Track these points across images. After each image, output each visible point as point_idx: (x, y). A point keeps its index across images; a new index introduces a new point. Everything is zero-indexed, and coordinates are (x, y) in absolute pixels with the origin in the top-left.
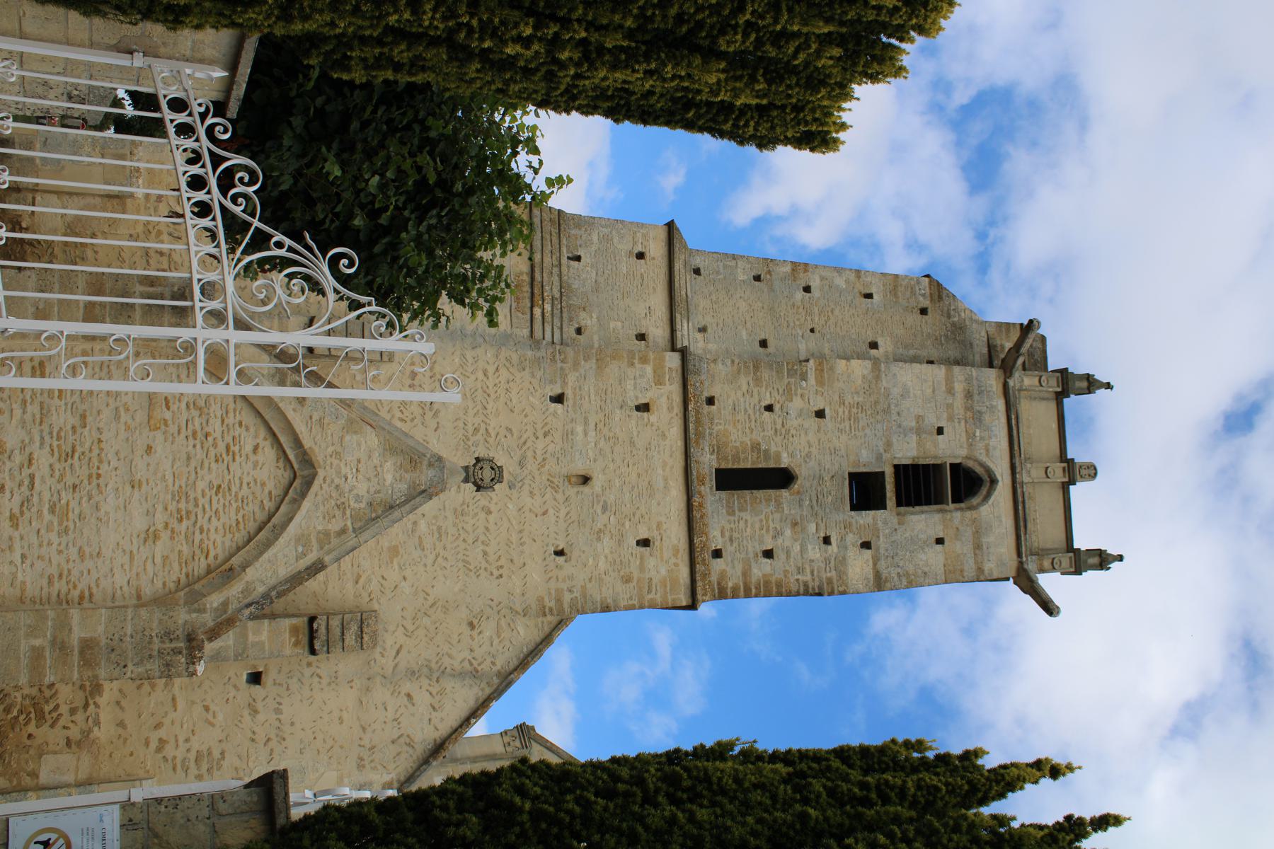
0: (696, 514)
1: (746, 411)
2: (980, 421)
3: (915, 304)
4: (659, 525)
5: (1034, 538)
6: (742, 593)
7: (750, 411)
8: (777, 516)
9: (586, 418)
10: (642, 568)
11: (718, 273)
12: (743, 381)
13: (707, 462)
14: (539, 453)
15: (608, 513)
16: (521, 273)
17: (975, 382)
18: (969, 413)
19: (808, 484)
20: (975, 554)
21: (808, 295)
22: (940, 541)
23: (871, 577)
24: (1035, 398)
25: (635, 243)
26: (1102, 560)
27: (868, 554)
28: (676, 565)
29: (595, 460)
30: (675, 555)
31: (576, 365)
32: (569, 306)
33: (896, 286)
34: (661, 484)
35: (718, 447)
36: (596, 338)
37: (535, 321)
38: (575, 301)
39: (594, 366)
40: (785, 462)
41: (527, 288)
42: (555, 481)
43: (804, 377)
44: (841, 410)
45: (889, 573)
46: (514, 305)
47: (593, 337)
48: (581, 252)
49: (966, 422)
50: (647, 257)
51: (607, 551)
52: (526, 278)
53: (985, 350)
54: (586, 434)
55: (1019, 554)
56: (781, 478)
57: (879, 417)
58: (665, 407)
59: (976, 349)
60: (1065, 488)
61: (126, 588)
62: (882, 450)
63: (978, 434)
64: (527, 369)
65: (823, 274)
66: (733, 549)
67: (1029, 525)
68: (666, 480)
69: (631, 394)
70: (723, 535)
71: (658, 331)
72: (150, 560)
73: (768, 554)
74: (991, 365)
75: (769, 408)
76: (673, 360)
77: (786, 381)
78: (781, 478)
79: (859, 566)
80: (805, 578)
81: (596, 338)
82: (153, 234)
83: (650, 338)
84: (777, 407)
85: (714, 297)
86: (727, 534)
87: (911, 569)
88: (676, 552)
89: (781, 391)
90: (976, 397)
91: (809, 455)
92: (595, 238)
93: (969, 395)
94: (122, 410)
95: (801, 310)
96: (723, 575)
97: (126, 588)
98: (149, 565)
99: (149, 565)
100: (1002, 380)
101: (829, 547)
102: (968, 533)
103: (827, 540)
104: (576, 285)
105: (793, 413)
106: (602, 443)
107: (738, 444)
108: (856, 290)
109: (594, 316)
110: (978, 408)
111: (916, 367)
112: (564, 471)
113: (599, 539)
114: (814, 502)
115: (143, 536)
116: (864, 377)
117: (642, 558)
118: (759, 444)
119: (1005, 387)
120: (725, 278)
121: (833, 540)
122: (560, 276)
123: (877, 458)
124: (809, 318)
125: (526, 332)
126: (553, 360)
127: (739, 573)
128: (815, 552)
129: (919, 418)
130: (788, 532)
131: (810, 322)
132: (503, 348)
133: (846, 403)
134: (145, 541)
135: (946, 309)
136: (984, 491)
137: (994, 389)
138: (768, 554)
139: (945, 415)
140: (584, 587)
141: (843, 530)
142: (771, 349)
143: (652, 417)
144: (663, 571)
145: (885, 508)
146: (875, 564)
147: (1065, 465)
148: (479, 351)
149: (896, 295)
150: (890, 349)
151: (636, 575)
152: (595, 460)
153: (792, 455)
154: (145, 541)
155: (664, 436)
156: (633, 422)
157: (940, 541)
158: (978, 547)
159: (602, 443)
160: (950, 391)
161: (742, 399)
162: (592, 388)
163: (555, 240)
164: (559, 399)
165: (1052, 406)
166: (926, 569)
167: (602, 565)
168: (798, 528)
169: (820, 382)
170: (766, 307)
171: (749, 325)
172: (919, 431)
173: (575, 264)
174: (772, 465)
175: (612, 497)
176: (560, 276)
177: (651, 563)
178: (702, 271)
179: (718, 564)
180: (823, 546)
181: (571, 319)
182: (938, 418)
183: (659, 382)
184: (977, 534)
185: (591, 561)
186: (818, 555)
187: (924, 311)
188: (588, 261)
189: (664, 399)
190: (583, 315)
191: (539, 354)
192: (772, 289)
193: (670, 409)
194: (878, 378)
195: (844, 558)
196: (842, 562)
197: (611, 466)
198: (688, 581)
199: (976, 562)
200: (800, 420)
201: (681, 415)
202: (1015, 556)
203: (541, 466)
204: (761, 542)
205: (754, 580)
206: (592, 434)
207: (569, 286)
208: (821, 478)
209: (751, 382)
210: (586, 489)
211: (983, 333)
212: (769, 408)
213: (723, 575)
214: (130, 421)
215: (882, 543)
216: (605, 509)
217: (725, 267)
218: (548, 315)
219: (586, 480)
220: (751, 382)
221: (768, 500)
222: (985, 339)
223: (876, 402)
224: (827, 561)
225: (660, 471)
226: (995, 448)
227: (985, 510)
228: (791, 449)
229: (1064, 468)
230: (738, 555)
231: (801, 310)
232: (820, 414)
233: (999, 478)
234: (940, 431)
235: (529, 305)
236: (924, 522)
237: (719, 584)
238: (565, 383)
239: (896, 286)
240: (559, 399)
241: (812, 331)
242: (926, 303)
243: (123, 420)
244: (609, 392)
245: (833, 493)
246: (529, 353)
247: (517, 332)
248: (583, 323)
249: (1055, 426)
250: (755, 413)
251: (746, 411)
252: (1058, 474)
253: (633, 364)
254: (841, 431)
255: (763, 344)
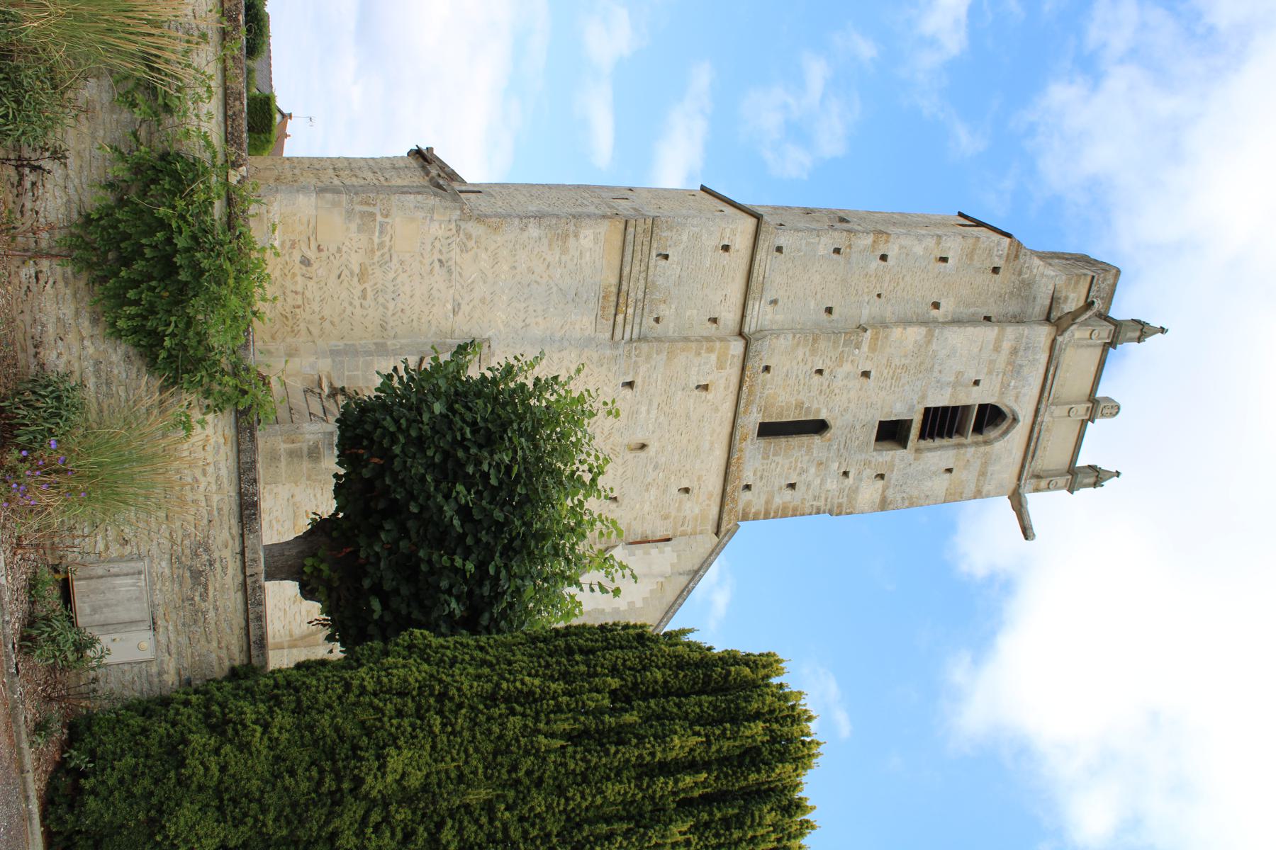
0: (733, 468)
1: (797, 376)
2: (1018, 373)
3: (989, 265)
4: (699, 478)
5: (1040, 461)
6: (762, 516)
7: (801, 377)
8: (806, 458)
9: (651, 400)
10: (679, 509)
11: (799, 250)
12: (800, 353)
13: (752, 419)
14: (606, 429)
15: (658, 471)
16: (610, 286)
17: (1024, 340)
18: (1009, 367)
19: (840, 432)
20: (978, 480)
21: (883, 263)
22: (949, 470)
23: (878, 501)
24: (1082, 346)
25: (722, 238)
26: (1097, 476)
27: (880, 483)
28: (709, 505)
29: (653, 432)
30: (709, 499)
31: (648, 358)
32: (651, 301)
33: (974, 249)
34: (707, 445)
35: (765, 407)
36: (672, 325)
37: (627, 244)
38: (657, 296)
39: (665, 358)
40: (823, 415)
41: (613, 298)
42: (617, 449)
43: (858, 346)
44: (886, 371)
45: (895, 498)
46: (600, 313)
47: (670, 326)
48: (669, 252)
49: (1004, 374)
50: (732, 250)
51: (652, 498)
52: (614, 289)
53: (1047, 302)
54: (648, 412)
55: (1019, 479)
56: (819, 427)
57: (921, 376)
58: (722, 386)
59: (1039, 301)
60: (1083, 424)
61: (282, 631)
62: (915, 402)
63: (1012, 384)
64: (605, 366)
65: (903, 243)
66: (761, 484)
67: (1038, 453)
68: (712, 443)
69: (695, 378)
70: (755, 474)
71: (729, 317)
72: (298, 614)
73: (792, 486)
74: (1048, 319)
75: (820, 372)
76: (737, 347)
77: (840, 350)
78: (819, 427)
79: (870, 492)
80: (819, 504)
81: (672, 325)
82: (289, 277)
83: (721, 322)
84: (826, 373)
85: (790, 273)
86: (759, 474)
87: (915, 493)
88: (710, 496)
89: (834, 358)
90: (1021, 353)
91: (846, 410)
92: (685, 238)
93: (1014, 351)
94: (274, 522)
95: (873, 278)
96: (749, 504)
97: (282, 631)
98: (298, 616)
99: (298, 616)
100: (1052, 336)
101: (847, 480)
102: (976, 465)
103: (846, 474)
104: (660, 281)
105: (840, 376)
106: (662, 418)
107: (784, 404)
108: (932, 256)
109: (673, 307)
110: (1020, 362)
111: (970, 330)
112: (626, 442)
113: (647, 490)
114: (842, 446)
115: (292, 599)
116: (916, 342)
117: (680, 502)
118: (803, 403)
119: (1054, 341)
120: (805, 255)
121: (851, 475)
122: (646, 279)
123: (909, 410)
124: (878, 285)
125: (608, 335)
126: (629, 356)
127: (763, 502)
128: (832, 484)
129: (959, 374)
130: (813, 470)
131: (878, 288)
132: (586, 350)
133: (893, 366)
134: (294, 602)
135: (1019, 267)
136: (1004, 426)
137: (1042, 345)
138: (792, 486)
139: (985, 370)
140: (629, 524)
141: (862, 468)
142: (835, 315)
143: (710, 396)
144: (697, 511)
145: (905, 447)
146: (884, 491)
147: (1090, 405)
148: (564, 353)
149: (971, 259)
150: (951, 309)
151: (673, 514)
152: (653, 432)
153: (831, 410)
154: (294, 602)
155: (717, 410)
156: (692, 401)
157: (949, 470)
158: (983, 474)
159: (662, 418)
160: (997, 349)
161: (796, 368)
162: (660, 376)
163: (646, 248)
164: (630, 385)
165: (1098, 351)
166: (929, 493)
167: (647, 508)
168: (822, 467)
169: (873, 349)
170: (839, 279)
171: (819, 296)
172: (955, 385)
173: (663, 262)
174: (811, 418)
175: (664, 459)
176: (646, 279)
177: (688, 505)
178: (784, 250)
179: (747, 495)
180: (841, 478)
181: (651, 312)
182: (977, 373)
183: (720, 367)
184: (985, 464)
185: (638, 506)
186: (835, 487)
187: (996, 270)
188: (676, 259)
189: (723, 380)
190: (662, 306)
191: (616, 353)
192: (848, 262)
193: (727, 388)
194: (929, 342)
195: (857, 488)
196: (855, 490)
197: (667, 436)
198: (716, 517)
199: (977, 486)
200: (845, 382)
201: (735, 392)
202: (1015, 480)
203: (607, 438)
204: (787, 478)
205: (774, 507)
206: (654, 412)
207: (653, 283)
208: (853, 427)
209: (807, 354)
210: (642, 454)
211: (1051, 287)
212: (820, 372)
213: (749, 504)
214: (280, 529)
215: (894, 477)
216: (656, 467)
217: (808, 244)
218: (629, 317)
219: (643, 446)
220: (807, 354)
221: (801, 447)
222: (1051, 292)
223: (922, 363)
224: (841, 490)
225: (708, 438)
226: (1025, 395)
227: (998, 446)
228: (831, 405)
229: (1088, 408)
230: (765, 488)
231: (873, 278)
232: (866, 374)
233: (1021, 418)
234: (977, 383)
235: (613, 312)
236: (940, 454)
237: (744, 510)
238: (637, 373)
239: (974, 249)
240: (630, 385)
241: (879, 296)
242: (998, 262)
243: (275, 529)
244: (674, 378)
245: (861, 438)
246: (608, 352)
247: (601, 336)
248: (661, 314)
249: (1093, 369)
250: (805, 378)
251: (797, 376)
252: (1081, 410)
253: (699, 354)
254: (881, 388)
255: (829, 310)
